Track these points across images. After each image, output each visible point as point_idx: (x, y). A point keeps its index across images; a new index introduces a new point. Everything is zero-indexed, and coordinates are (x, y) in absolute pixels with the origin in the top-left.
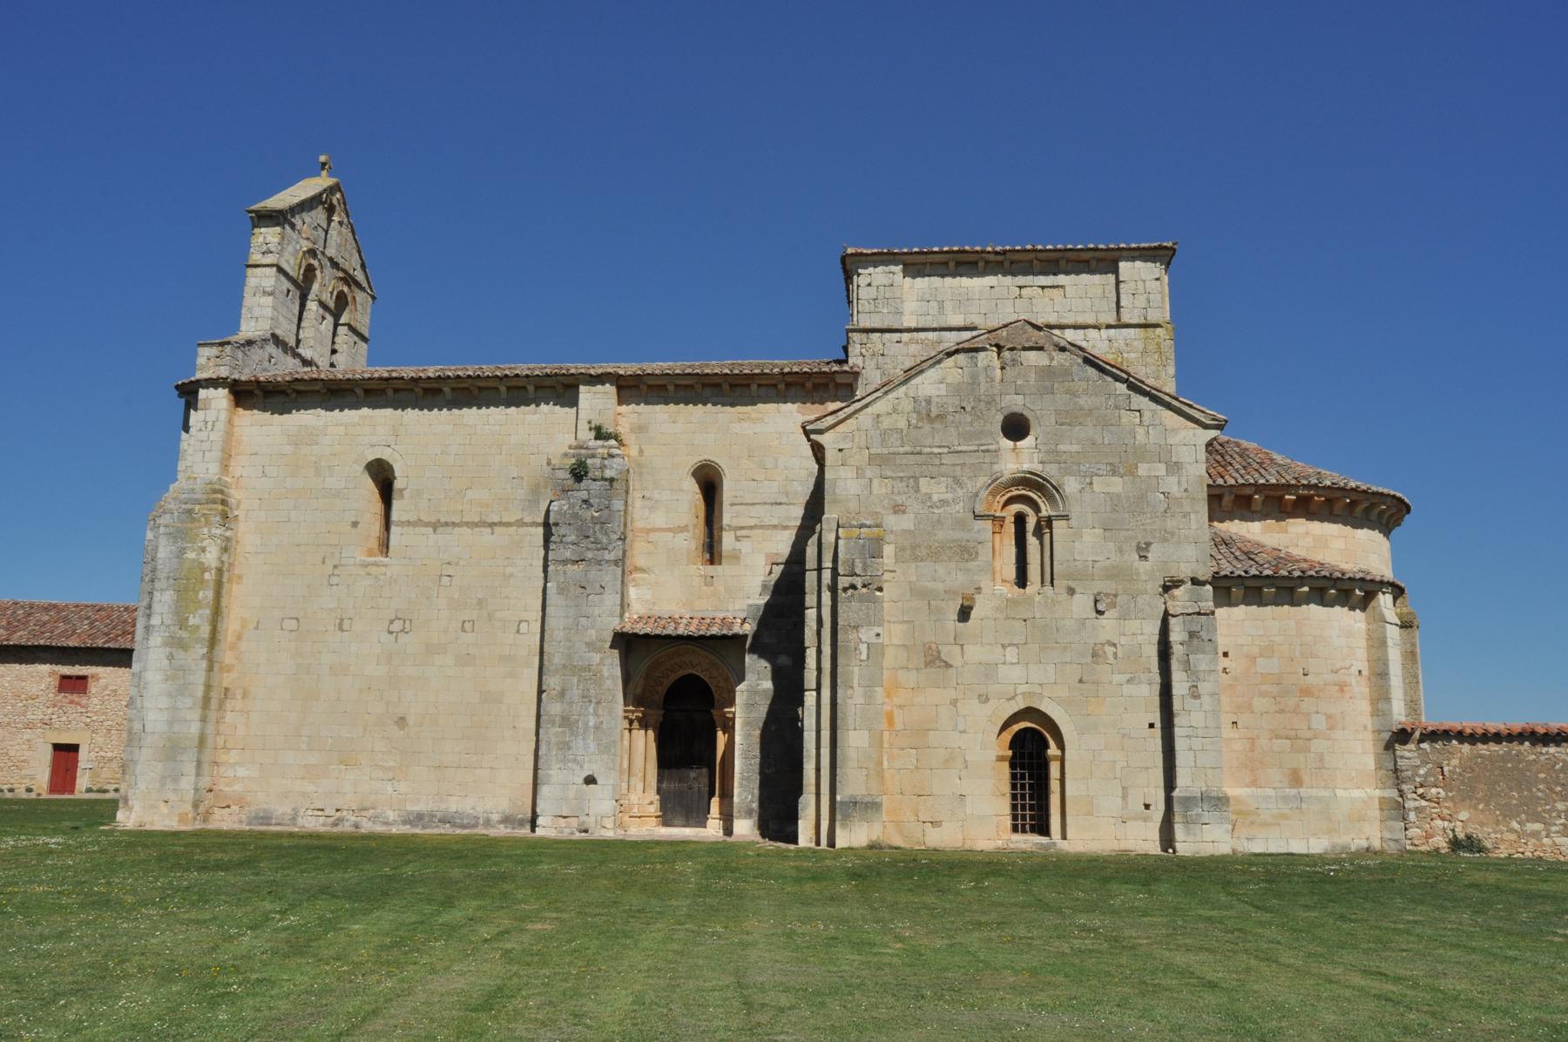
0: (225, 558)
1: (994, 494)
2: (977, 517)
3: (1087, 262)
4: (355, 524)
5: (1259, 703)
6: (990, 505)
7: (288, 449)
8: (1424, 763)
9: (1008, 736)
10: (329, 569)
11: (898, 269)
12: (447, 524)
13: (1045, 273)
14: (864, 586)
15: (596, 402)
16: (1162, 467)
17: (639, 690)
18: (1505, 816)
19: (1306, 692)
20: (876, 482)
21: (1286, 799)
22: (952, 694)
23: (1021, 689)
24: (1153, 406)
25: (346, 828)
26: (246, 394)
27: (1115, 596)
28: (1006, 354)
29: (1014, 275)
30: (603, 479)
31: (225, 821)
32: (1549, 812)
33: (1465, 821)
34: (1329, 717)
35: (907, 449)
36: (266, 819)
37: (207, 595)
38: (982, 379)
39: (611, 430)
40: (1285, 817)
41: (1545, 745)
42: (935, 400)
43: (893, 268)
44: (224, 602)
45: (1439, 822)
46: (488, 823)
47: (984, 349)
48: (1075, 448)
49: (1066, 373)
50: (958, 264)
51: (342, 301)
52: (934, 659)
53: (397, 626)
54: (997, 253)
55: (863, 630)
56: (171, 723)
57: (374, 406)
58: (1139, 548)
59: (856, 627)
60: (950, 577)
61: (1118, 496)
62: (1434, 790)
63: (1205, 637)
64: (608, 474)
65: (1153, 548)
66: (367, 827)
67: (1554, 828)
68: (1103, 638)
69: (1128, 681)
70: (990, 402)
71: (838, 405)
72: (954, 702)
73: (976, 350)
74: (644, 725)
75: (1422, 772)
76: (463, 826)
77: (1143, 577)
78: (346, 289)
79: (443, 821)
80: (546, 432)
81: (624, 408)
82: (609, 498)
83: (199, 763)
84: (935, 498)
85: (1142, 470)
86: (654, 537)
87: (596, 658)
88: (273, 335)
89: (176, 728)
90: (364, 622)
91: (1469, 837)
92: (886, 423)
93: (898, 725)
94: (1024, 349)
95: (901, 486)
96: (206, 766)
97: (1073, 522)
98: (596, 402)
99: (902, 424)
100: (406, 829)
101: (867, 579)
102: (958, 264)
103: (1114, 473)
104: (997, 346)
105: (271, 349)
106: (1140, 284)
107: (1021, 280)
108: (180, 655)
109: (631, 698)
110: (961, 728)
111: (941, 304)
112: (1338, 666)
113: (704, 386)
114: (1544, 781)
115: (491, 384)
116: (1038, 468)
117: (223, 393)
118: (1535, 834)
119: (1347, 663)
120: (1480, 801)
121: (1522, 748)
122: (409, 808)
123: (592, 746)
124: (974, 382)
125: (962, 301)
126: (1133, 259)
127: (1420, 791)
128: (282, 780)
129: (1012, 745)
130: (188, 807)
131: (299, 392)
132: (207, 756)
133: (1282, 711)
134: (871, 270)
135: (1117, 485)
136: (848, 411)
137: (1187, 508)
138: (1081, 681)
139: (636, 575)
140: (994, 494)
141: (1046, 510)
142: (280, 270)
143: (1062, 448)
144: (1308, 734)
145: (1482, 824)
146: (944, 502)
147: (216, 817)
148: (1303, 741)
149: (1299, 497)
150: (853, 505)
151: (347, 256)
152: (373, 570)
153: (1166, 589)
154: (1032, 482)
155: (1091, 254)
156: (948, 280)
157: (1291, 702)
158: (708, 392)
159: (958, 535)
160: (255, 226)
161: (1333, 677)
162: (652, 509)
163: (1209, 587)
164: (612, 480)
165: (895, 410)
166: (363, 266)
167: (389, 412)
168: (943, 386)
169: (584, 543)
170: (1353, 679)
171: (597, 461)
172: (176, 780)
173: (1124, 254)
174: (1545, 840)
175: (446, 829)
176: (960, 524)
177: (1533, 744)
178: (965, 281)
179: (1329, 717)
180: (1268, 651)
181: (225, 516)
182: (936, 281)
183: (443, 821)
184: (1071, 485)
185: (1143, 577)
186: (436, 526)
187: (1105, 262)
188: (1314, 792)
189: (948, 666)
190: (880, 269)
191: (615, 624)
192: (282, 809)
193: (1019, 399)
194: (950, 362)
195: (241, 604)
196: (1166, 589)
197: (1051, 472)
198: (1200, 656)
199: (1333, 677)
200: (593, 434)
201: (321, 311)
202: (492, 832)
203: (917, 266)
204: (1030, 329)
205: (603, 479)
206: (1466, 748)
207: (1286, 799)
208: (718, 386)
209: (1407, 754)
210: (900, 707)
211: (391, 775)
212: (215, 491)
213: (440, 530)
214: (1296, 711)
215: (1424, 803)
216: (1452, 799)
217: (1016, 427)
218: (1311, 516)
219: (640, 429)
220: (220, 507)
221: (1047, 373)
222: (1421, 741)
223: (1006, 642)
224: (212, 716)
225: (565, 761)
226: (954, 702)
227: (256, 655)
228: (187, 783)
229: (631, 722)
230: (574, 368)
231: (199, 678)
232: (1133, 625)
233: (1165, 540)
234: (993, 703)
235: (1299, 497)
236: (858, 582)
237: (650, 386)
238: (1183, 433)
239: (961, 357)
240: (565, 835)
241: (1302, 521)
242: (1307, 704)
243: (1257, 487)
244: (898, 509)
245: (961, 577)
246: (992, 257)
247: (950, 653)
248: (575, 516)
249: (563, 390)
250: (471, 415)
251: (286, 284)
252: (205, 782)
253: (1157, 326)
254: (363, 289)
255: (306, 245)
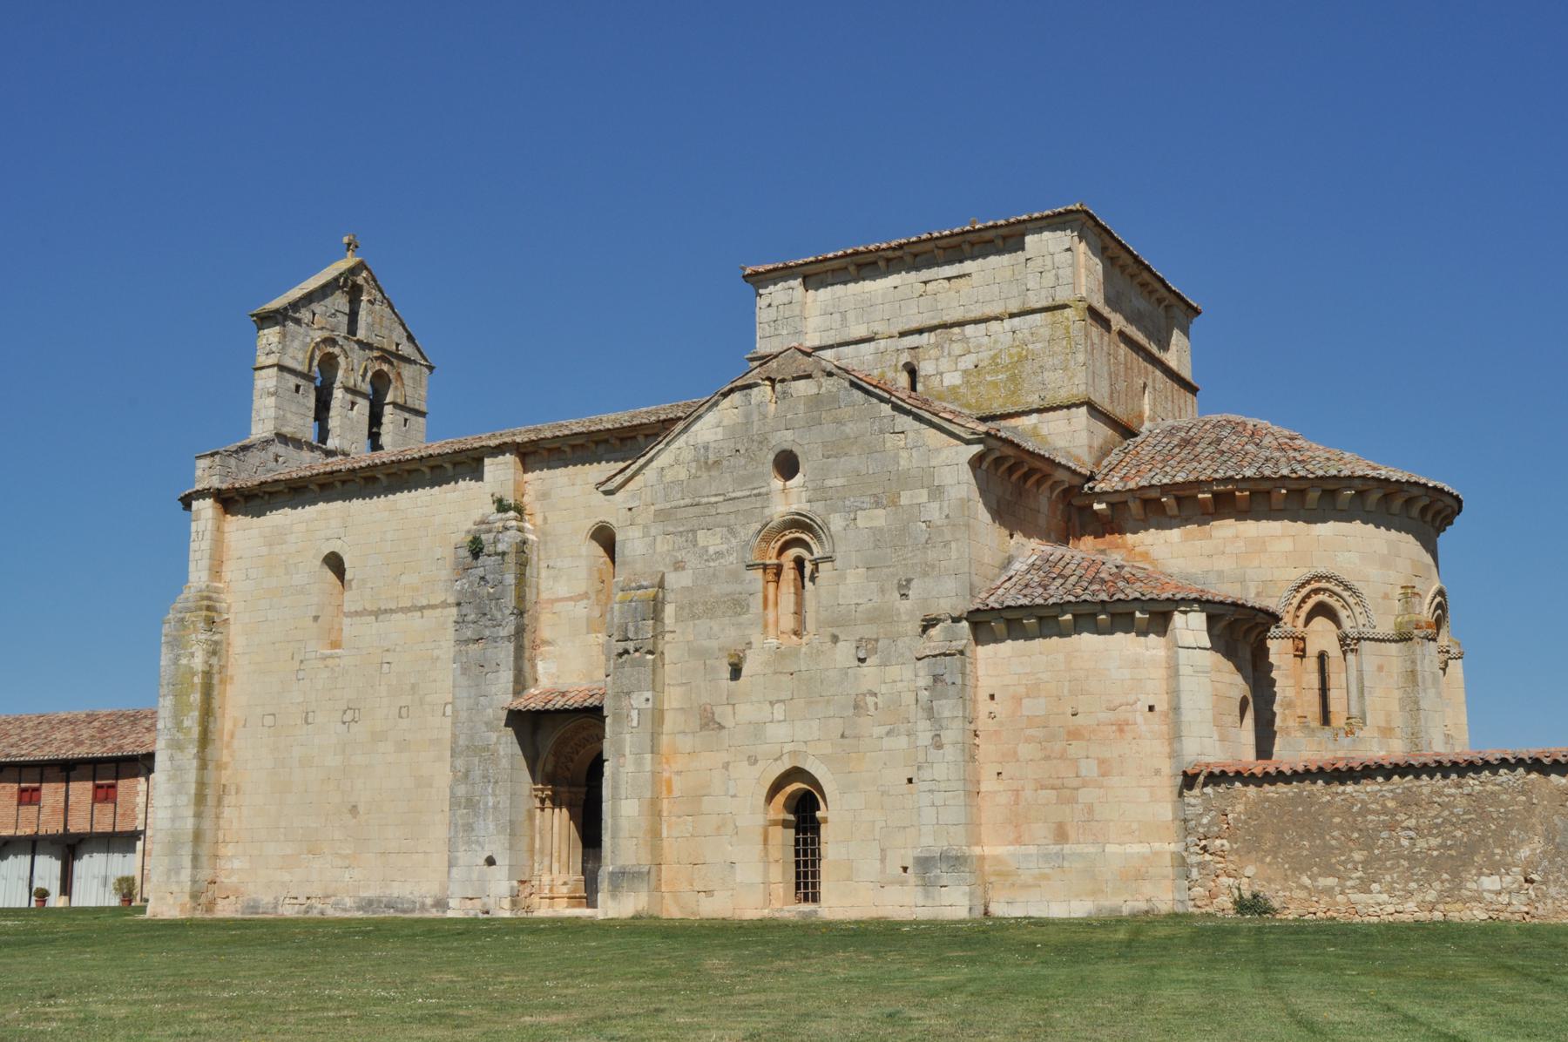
0: (214, 660)
1: (767, 540)
2: (750, 567)
3: (991, 241)
4: (316, 618)
5: (1025, 750)
6: (764, 552)
7: (264, 551)
8: (1207, 810)
9: (780, 799)
10: (296, 665)
11: (796, 283)
12: (386, 611)
13: (950, 262)
14: (636, 650)
15: (500, 472)
16: (925, 492)
17: (549, 768)
18: (1294, 870)
19: (1074, 734)
20: (659, 539)
21: (1047, 857)
22: (724, 757)
23: (787, 748)
24: (917, 424)
25: (315, 914)
26: (232, 501)
27: (877, 640)
28: (778, 386)
29: (918, 269)
30: (497, 554)
31: (226, 910)
32: (1343, 863)
33: (1252, 877)
34: (1102, 762)
35: (688, 501)
36: (254, 908)
37: (196, 698)
38: (755, 417)
39: (512, 501)
40: (1046, 877)
41: (1342, 783)
42: (712, 445)
43: (792, 283)
44: (216, 703)
45: (1224, 880)
46: (423, 907)
47: (756, 385)
48: (841, 482)
49: (834, 399)
50: (859, 266)
51: (380, 383)
52: (709, 722)
53: (348, 717)
54: (894, 249)
55: (634, 696)
56: (173, 820)
57: (328, 500)
58: (900, 586)
59: (628, 694)
60: (723, 634)
61: (881, 530)
62: (1218, 842)
63: (949, 681)
64: (501, 547)
65: (914, 584)
66: (331, 913)
67: (1349, 883)
68: (864, 689)
69: (888, 734)
70: (763, 441)
71: (622, 465)
72: (726, 766)
73: (749, 387)
74: (556, 802)
75: (1205, 821)
76: (404, 911)
77: (904, 618)
78: (385, 367)
79: (388, 906)
80: (456, 507)
81: (529, 476)
82: (502, 573)
83: (195, 858)
84: (711, 550)
85: (904, 500)
86: (558, 607)
87: (494, 736)
88: (277, 435)
89: (177, 825)
90: (316, 719)
91: (1255, 896)
92: (669, 476)
93: (676, 793)
94: (794, 379)
95: (681, 540)
96: (204, 860)
97: (838, 564)
98: (500, 472)
99: (683, 475)
100: (360, 915)
101: (638, 643)
102: (859, 266)
103: (878, 504)
104: (772, 380)
105: (278, 448)
106: (1048, 259)
107: (926, 274)
108: (178, 755)
109: (539, 775)
110: (732, 792)
111: (843, 314)
112: (1117, 703)
113: (597, 443)
114: (1340, 827)
115: (413, 466)
116: (804, 507)
117: (209, 502)
118: (1328, 891)
119: (1131, 698)
120: (1267, 853)
121: (1314, 788)
122: (362, 894)
123: (491, 826)
124: (748, 422)
125: (865, 307)
126: (1040, 230)
127: (1203, 843)
128: (267, 874)
129: (787, 807)
130: (187, 898)
131: (270, 494)
132: (205, 850)
133: (1047, 758)
134: (771, 288)
135: (880, 518)
136: (634, 467)
137: (948, 537)
138: (843, 736)
139: (544, 649)
140: (767, 540)
141: (818, 552)
142: (282, 368)
143: (829, 483)
144: (1076, 783)
145: (1269, 881)
146: (719, 554)
147: (219, 907)
148: (1079, 786)
149: (1216, 495)
150: (639, 567)
151: (385, 332)
152: (330, 662)
153: (925, 629)
154: (799, 523)
155: (992, 233)
156: (851, 286)
157: (1058, 746)
158: (602, 448)
159: (728, 588)
160: (260, 329)
161: (1111, 716)
162: (556, 579)
163: (965, 624)
164: (504, 554)
165: (677, 461)
166: (410, 338)
167: (339, 503)
168: (720, 430)
169: (483, 621)
170: (1140, 717)
171: (491, 536)
172: (178, 873)
173: (1029, 225)
174: (1340, 898)
175: (391, 913)
176: (734, 577)
177: (1327, 783)
178: (868, 286)
179: (1102, 762)
180: (1033, 691)
181: (211, 622)
182: (839, 288)
183: (388, 906)
184: (836, 523)
185: (904, 618)
186: (377, 613)
187: (1007, 239)
188: (1079, 848)
189: (721, 727)
190: (780, 285)
191: (509, 701)
192: (266, 899)
193: (789, 435)
194: (726, 403)
195: (235, 702)
196: (925, 629)
197: (816, 511)
198: (944, 702)
199: (1111, 716)
200: (494, 508)
201: (349, 397)
202: (427, 915)
203: (816, 276)
204: (799, 356)
205: (497, 554)
206: (1252, 790)
207: (1047, 857)
208: (606, 441)
209: (1193, 801)
210: (679, 773)
211: (347, 862)
212: (203, 598)
213: (381, 617)
214: (1063, 756)
215: (1207, 857)
216: (1237, 851)
217: (787, 465)
218: (1242, 514)
219: (544, 496)
220: (204, 613)
221: (816, 402)
222: (1205, 785)
223: (774, 698)
224: (210, 811)
225: (469, 843)
226: (726, 766)
227: (245, 751)
228: (186, 875)
229: (542, 801)
230: (472, 442)
231: (191, 776)
232: (894, 671)
233: (926, 574)
234: (761, 764)
235: (1216, 495)
236: (631, 646)
237: (549, 450)
238: (945, 453)
239: (736, 396)
240: (471, 914)
241: (1231, 521)
242: (1075, 749)
243: (1165, 489)
244: (679, 566)
245: (732, 633)
246: (890, 254)
247: (723, 714)
248: (474, 593)
249: (467, 464)
250: (403, 499)
251: (292, 381)
252: (205, 874)
253: (1065, 306)
254: (415, 362)
255: (318, 336)
